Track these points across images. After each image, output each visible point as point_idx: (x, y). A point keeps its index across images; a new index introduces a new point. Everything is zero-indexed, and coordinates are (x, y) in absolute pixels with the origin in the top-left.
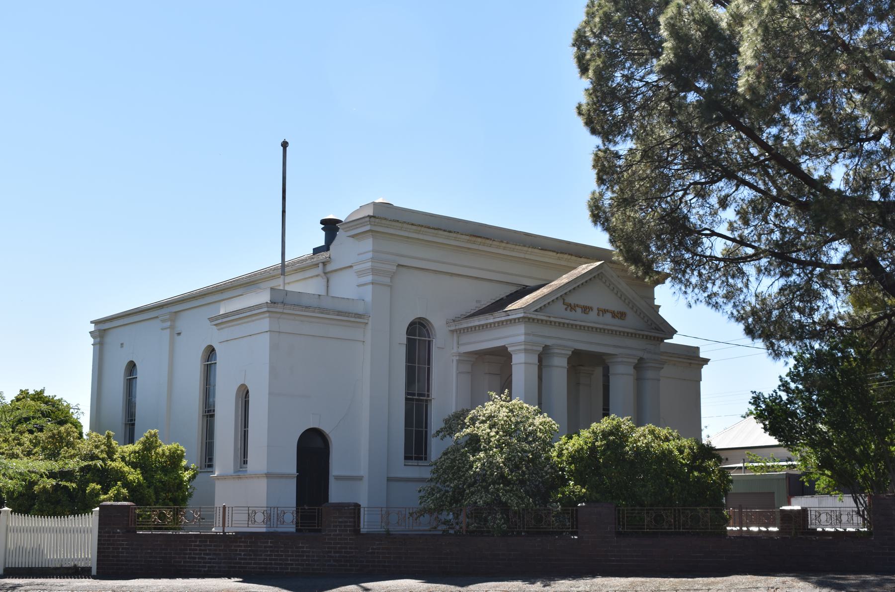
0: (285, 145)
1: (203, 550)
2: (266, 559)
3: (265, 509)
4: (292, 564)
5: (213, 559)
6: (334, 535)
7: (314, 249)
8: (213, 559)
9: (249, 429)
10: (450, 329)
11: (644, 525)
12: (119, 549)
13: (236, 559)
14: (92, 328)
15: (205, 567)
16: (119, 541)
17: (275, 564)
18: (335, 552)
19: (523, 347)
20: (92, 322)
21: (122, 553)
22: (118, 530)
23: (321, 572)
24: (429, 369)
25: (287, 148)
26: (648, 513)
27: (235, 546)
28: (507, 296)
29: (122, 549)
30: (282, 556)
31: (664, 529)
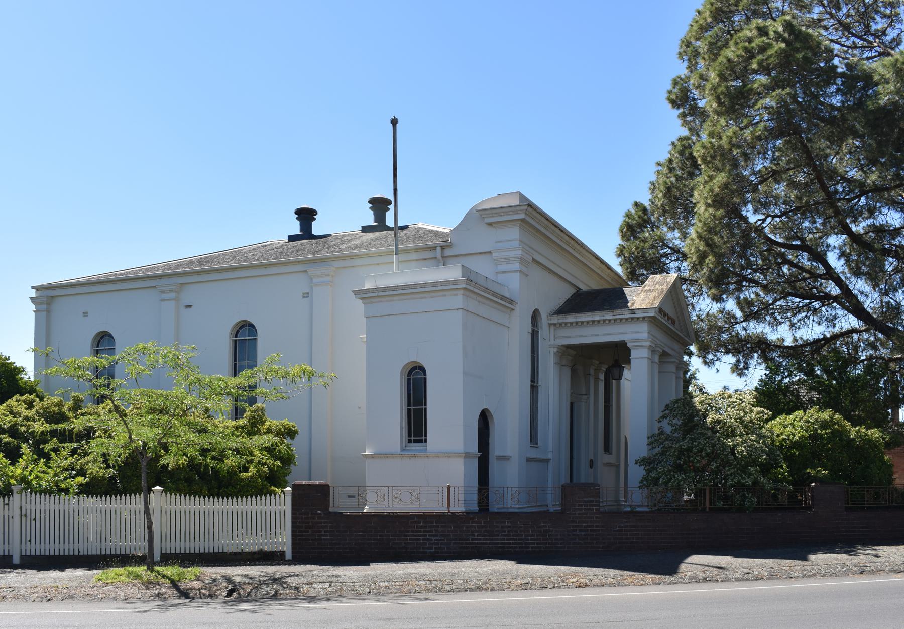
0: (394, 122)
1: (428, 531)
2: (504, 539)
3: (517, 489)
4: (533, 543)
5: (441, 540)
6: (579, 514)
7: (289, 237)
8: (441, 540)
9: (428, 407)
10: (550, 322)
11: (864, 501)
12: (321, 531)
13: (468, 539)
14: (33, 293)
15: (431, 548)
16: (321, 523)
17: (514, 543)
18: (580, 531)
19: (648, 343)
20: (33, 288)
21: (326, 535)
22: (319, 512)
23: (566, 550)
24: (235, 360)
25: (397, 125)
26: (868, 491)
27: (467, 527)
28: (571, 297)
29: (325, 531)
30: (522, 535)
31: (882, 504)
